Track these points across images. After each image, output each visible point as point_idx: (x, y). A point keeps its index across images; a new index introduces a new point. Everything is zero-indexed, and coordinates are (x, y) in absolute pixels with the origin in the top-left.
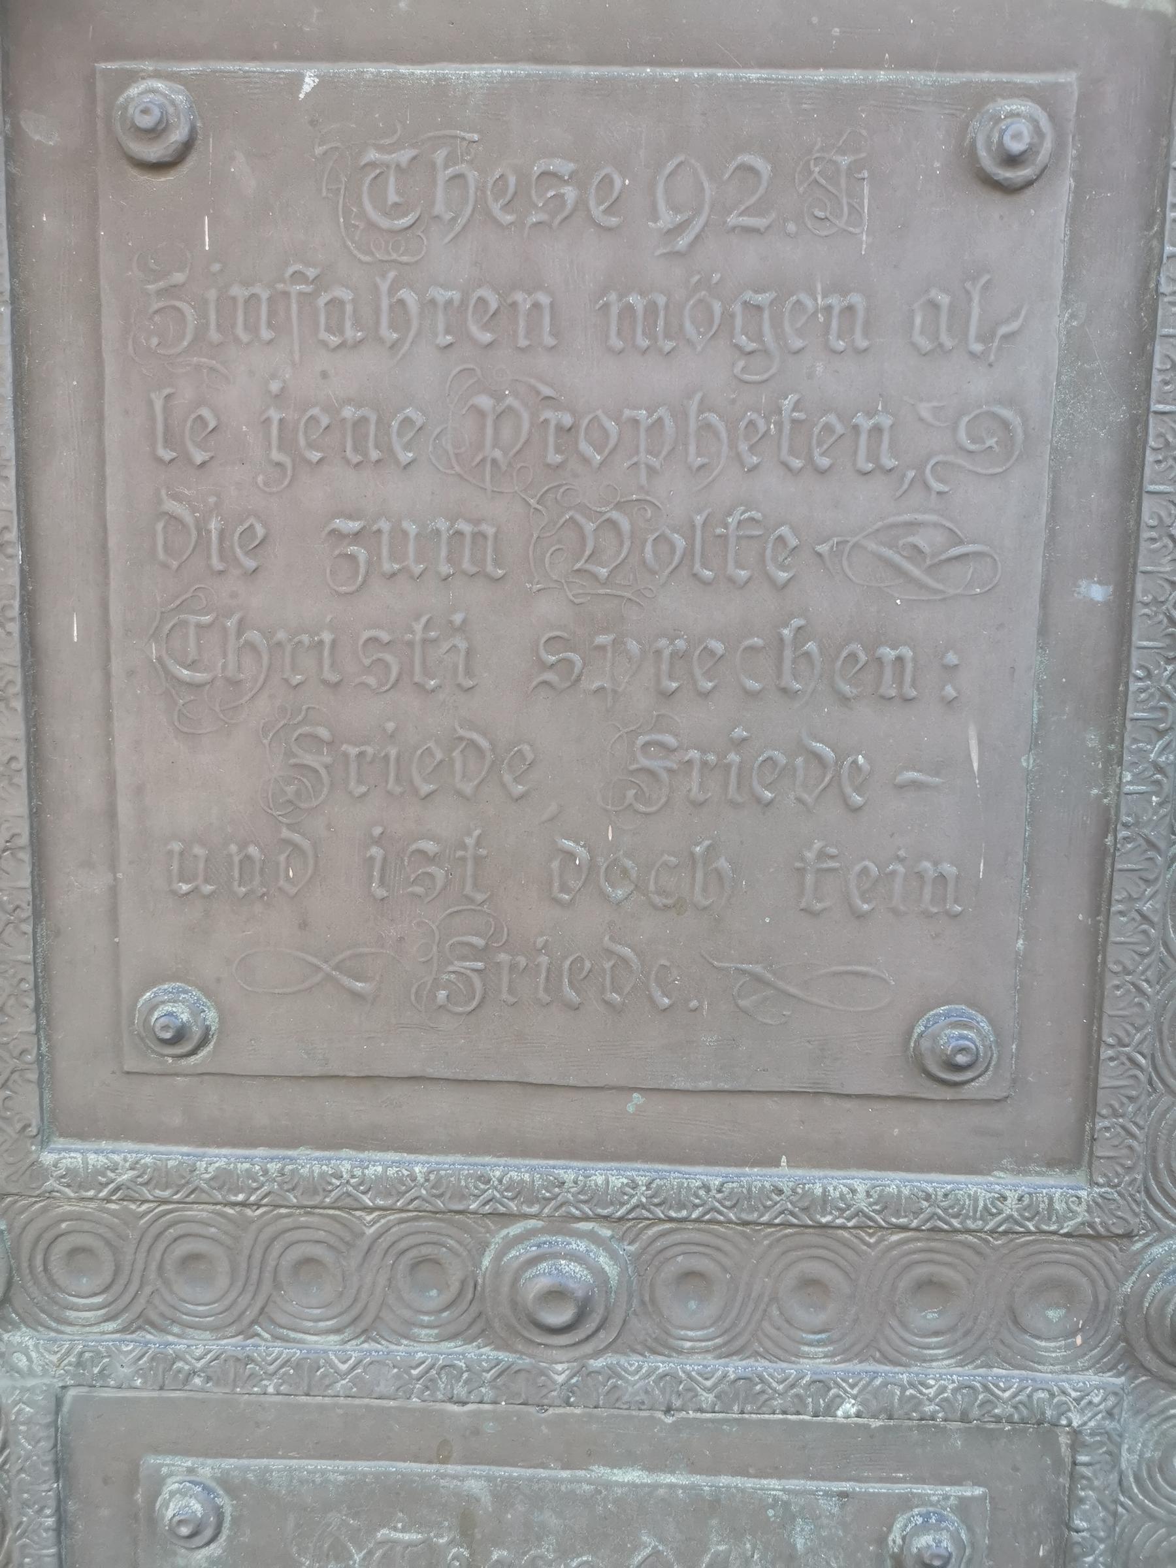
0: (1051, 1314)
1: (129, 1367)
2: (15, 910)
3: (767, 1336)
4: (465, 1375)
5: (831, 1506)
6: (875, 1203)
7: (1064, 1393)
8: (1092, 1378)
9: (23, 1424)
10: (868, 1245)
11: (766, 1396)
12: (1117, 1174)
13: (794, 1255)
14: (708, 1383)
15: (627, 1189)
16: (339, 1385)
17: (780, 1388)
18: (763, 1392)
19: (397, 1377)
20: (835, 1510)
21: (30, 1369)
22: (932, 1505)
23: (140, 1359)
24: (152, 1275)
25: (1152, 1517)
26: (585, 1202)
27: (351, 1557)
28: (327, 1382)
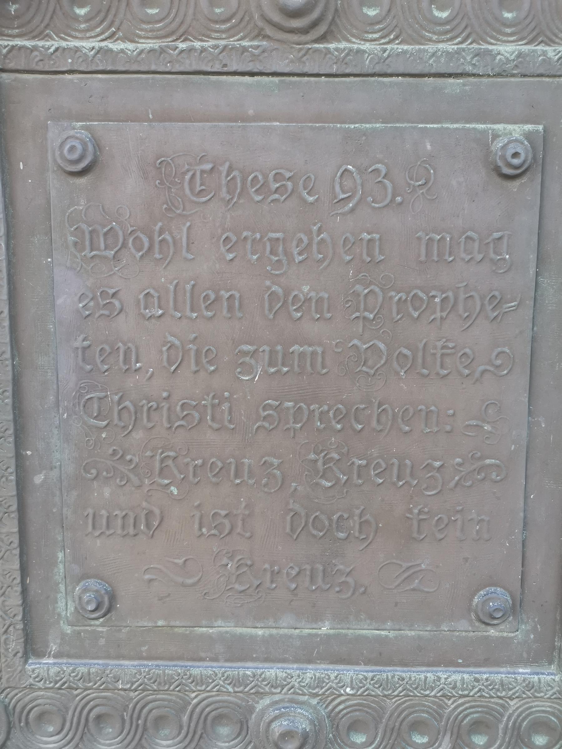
2: (10, 543)
24: (127, 718)
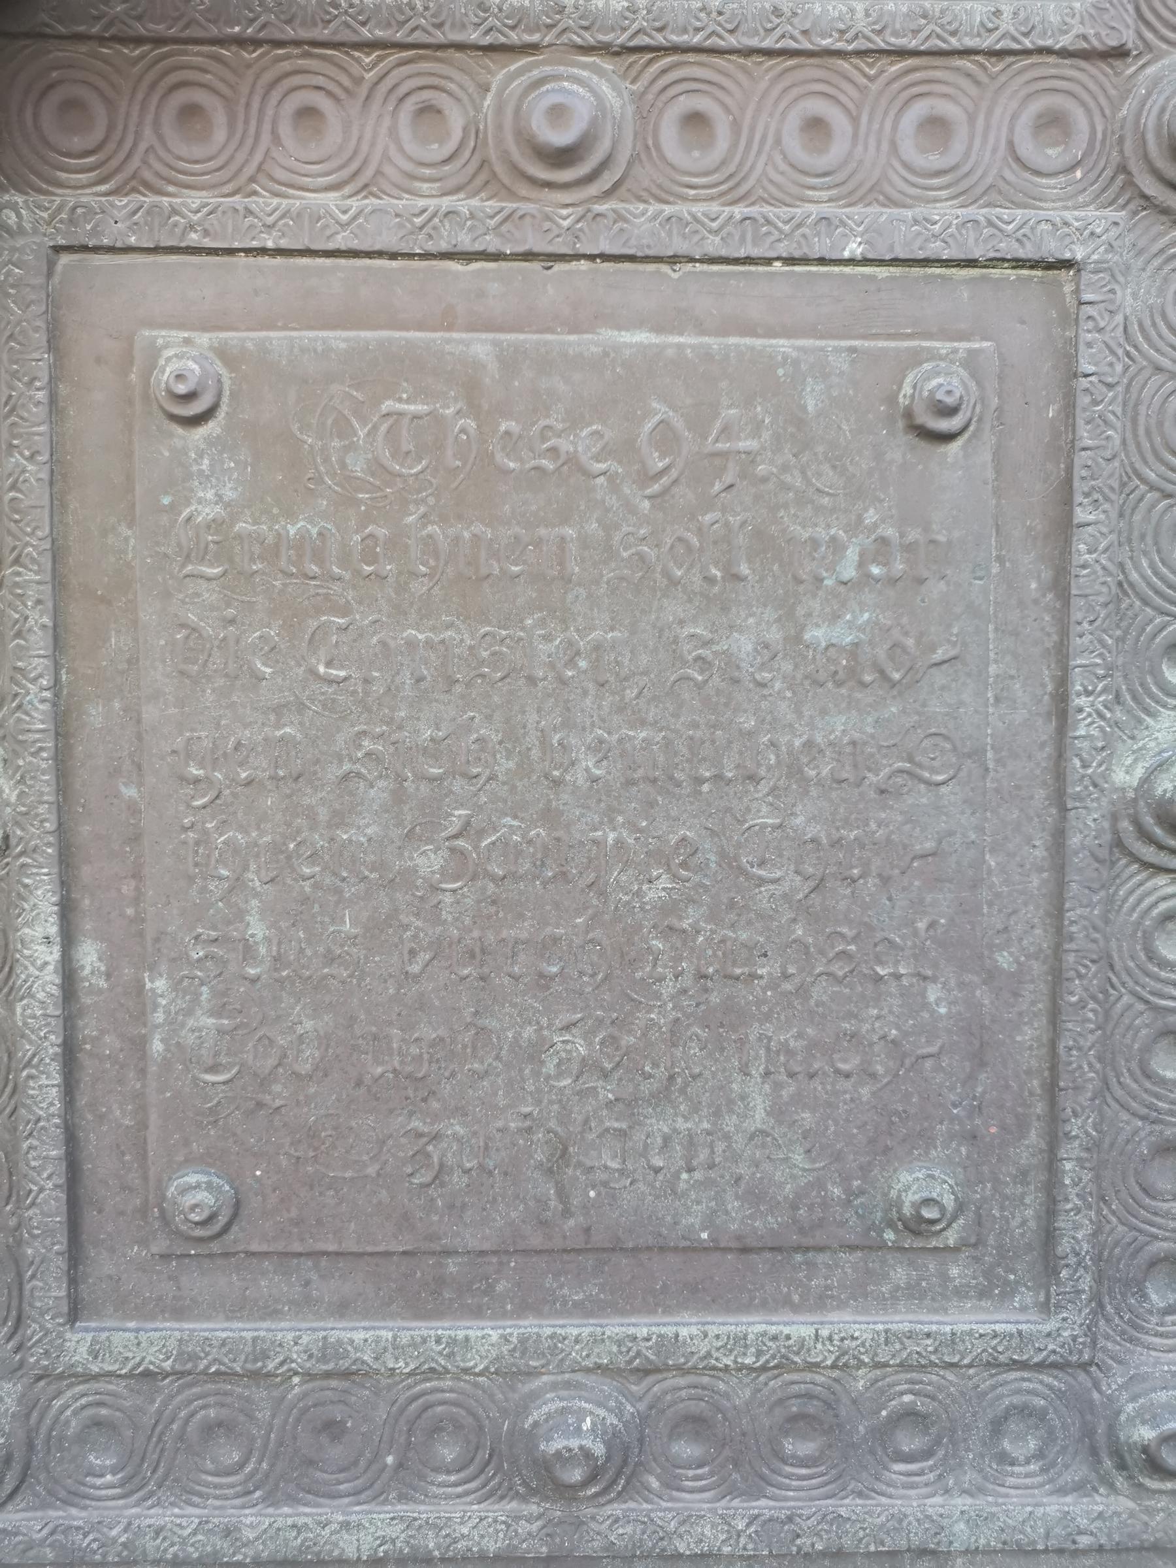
0: (1050, 152)
1: (123, 221)
3: (771, 181)
4: (469, 223)
5: (841, 363)
6: (874, 23)
7: (1066, 224)
8: (1091, 213)
9: (12, 286)
10: (865, 75)
11: (772, 238)
12: (1086, 966)
13: (795, 92)
14: (715, 225)
15: (628, 14)
16: (339, 237)
17: (787, 228)
18: (769, 233)
19: (401, 226)
20: (845, 367)
21: (20, 226)
22: (941, 358)
23: (135, 213)
25: (1159, 369)
26: (586, 28)
27: (355, 434)
28: (328, 232)
